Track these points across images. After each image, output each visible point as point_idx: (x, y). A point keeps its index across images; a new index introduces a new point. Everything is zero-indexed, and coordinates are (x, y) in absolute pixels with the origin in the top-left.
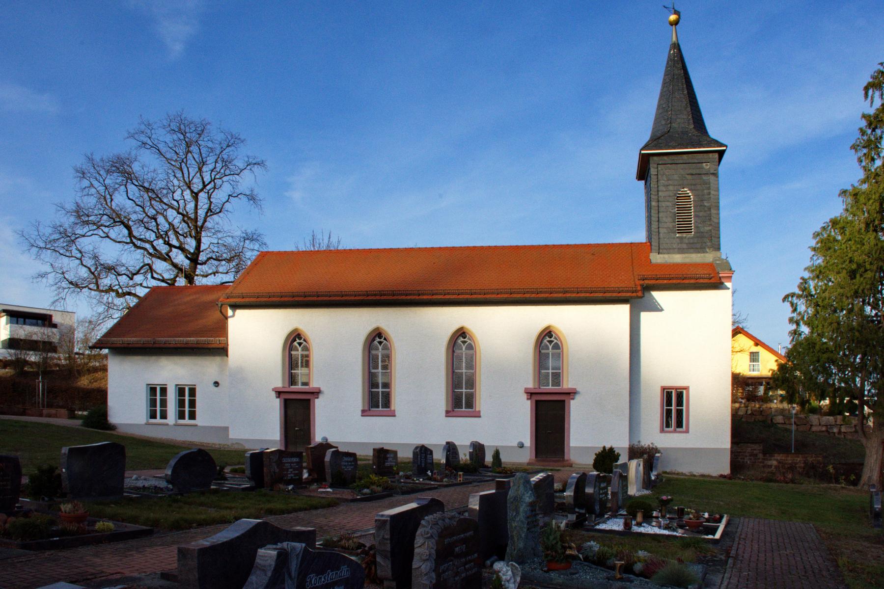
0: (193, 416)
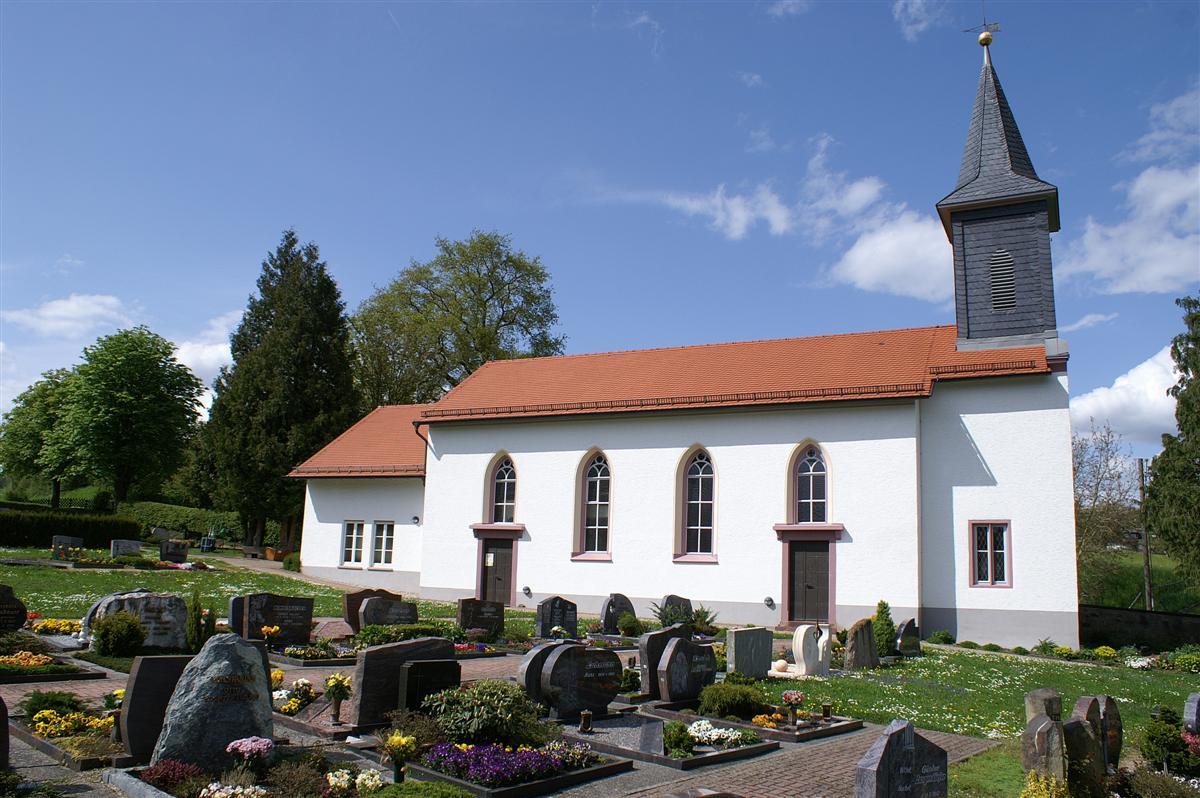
0: (388, 560)
